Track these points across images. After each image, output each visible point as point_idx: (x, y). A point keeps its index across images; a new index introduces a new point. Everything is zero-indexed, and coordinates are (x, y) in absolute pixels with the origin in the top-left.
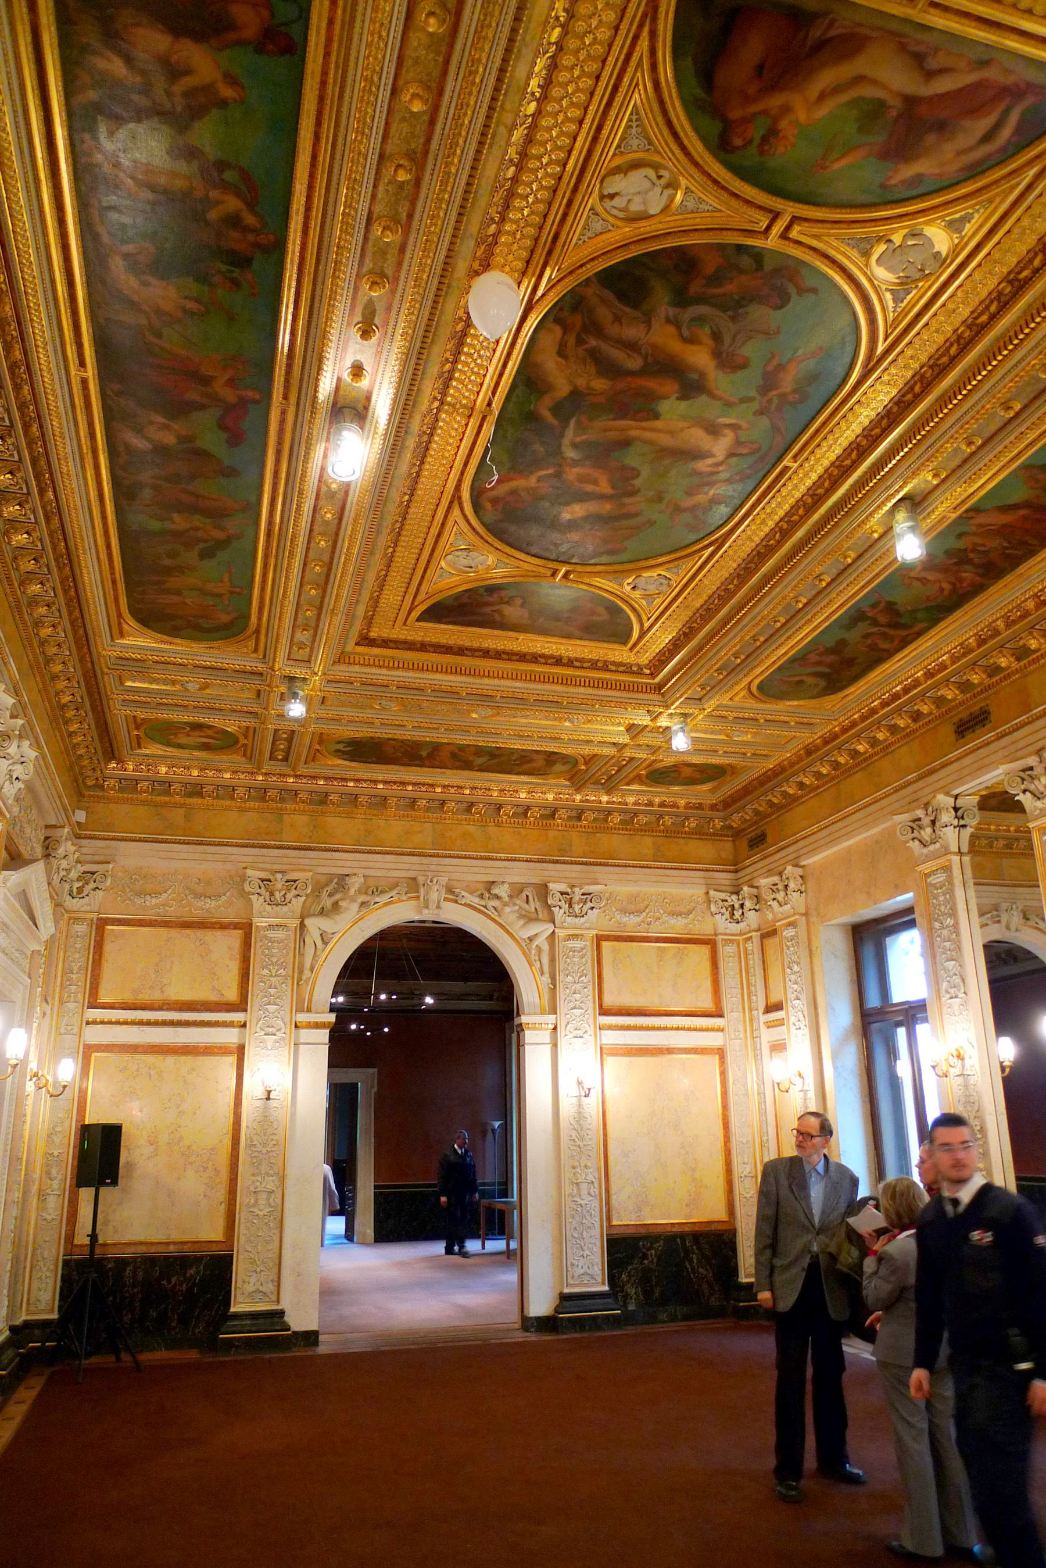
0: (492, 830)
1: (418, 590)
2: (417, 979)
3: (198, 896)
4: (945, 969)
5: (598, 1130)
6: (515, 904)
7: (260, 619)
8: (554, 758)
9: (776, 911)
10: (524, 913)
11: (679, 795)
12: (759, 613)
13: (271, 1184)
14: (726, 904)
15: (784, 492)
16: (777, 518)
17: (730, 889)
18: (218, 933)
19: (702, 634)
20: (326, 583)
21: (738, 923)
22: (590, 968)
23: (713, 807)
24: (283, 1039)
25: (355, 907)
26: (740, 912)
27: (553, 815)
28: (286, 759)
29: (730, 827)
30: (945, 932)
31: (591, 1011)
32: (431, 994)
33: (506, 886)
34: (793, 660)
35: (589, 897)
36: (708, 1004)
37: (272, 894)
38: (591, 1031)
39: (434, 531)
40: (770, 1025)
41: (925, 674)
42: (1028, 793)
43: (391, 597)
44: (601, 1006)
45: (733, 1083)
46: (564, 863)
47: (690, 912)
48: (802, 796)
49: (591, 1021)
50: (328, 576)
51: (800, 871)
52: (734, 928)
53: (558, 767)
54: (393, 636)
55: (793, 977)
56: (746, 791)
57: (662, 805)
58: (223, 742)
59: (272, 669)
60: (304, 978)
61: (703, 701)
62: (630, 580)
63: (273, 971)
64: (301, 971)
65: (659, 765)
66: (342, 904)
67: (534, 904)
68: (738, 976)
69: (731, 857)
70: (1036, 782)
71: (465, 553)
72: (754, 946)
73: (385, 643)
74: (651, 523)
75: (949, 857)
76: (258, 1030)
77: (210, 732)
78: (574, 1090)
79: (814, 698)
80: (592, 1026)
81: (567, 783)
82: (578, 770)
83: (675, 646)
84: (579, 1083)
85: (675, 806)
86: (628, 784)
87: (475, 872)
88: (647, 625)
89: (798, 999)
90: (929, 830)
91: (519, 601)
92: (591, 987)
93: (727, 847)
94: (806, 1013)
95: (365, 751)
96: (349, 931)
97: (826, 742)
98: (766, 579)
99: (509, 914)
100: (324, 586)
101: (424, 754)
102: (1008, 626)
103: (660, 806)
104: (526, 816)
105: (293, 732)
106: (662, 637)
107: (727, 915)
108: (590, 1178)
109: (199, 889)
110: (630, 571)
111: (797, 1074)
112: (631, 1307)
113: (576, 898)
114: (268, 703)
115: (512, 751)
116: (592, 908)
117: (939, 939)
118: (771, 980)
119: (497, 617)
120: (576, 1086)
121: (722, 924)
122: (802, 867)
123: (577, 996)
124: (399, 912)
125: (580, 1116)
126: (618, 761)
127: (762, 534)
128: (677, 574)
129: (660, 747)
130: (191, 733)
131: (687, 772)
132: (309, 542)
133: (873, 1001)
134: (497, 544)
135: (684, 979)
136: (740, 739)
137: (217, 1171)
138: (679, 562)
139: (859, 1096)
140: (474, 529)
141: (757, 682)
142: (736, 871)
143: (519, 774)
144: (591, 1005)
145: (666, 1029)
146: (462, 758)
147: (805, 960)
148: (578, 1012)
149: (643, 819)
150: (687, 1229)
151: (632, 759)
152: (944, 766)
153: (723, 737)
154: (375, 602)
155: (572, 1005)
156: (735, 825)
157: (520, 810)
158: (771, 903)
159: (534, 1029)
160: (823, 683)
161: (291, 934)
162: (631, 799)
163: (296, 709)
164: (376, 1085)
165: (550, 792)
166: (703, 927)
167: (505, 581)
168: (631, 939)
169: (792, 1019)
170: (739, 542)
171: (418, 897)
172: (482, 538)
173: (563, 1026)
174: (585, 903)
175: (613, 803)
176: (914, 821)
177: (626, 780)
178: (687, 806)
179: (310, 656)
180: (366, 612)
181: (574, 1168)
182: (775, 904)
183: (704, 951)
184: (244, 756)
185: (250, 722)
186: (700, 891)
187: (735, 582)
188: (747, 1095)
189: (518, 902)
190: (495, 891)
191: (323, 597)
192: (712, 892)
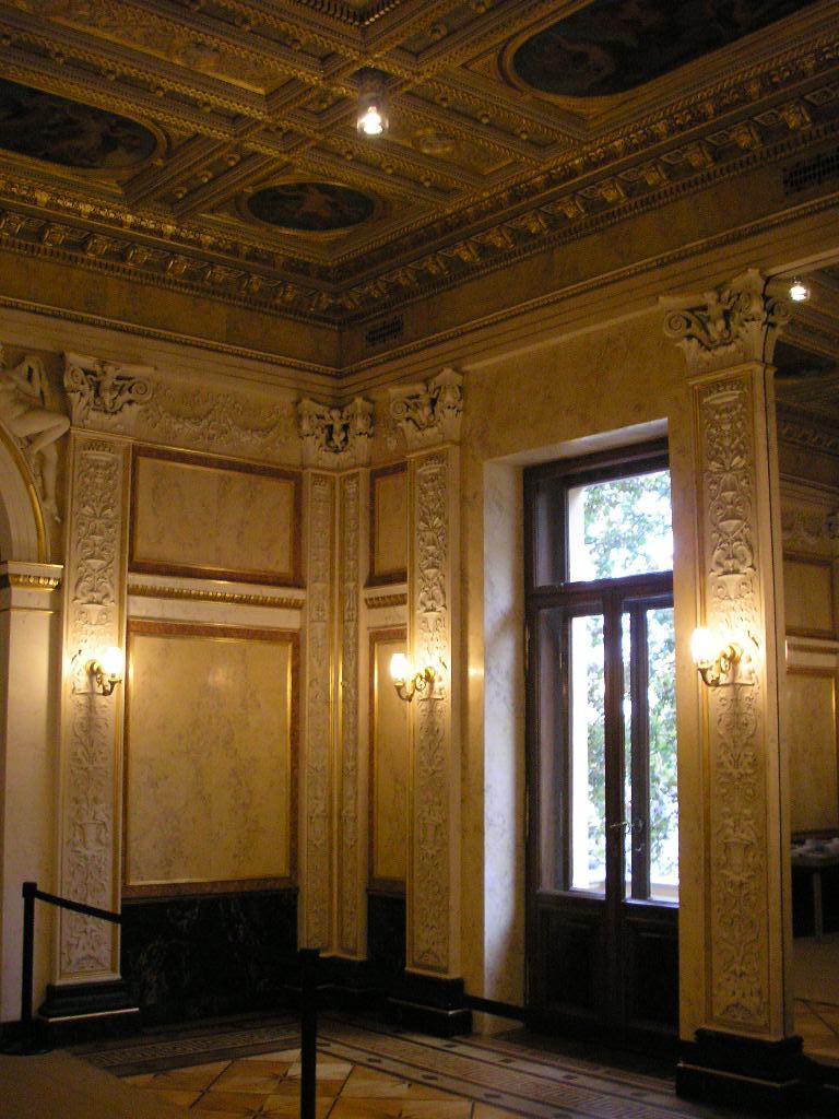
4: (721, 532)
5: (116, 745)
6: (10, 379)
10: (22, 396)
17: (330, 401)
23: (323, 274)
26: (343, 436)
27: (82, 246)
29: (343, 308)
30: (727, 477)
31: (116, 563)
35: (128, 384)
36: (282, 566)
38: (114, 596)
40: (373, 604)
41: (511, 195)
42: (411, 422)
46: (93, 324)
47: (270, 428)
49: (116, 580)
52: (329, 459)
53: (119, 157)
55: (429, 535)
61: (421, 59)
67: (40, 385)
68: (328, 531)
70: (420, 412)
72: (357, 489)
75: (747, 367)
78: (82, 682)
80: (116, 586)
81: (120, 192)
86: (212, 211)
89: (433, 566)
90: (427, 410)
92: (118, 526)
102: (718, 112)
103: (248, 257)
107: (323, 438)
108: (101, 816)
112: (150, 1001)
113: (108, 383)
116: (130, 402)
117: (713, 487)
118: (381, 542)
121: (314, 450)
123: (98, 538)
133: (543, 579)
139: (512, 709)
143: (47, 157)
144: (117, 555)
147: (453, 513)
148: (96, 563)
149: (220, 274)
150: (232, 889)
151: (255, 154)
152: (755, 232)
155: (88, 551)
156: (349, 305)
159: (28, 584)
173: (74, 581)
176: (411, 398)
183: (281, 491)
186: (287, 398)
188: (327, 702)
189: (15, 377)
192: (306, 402)
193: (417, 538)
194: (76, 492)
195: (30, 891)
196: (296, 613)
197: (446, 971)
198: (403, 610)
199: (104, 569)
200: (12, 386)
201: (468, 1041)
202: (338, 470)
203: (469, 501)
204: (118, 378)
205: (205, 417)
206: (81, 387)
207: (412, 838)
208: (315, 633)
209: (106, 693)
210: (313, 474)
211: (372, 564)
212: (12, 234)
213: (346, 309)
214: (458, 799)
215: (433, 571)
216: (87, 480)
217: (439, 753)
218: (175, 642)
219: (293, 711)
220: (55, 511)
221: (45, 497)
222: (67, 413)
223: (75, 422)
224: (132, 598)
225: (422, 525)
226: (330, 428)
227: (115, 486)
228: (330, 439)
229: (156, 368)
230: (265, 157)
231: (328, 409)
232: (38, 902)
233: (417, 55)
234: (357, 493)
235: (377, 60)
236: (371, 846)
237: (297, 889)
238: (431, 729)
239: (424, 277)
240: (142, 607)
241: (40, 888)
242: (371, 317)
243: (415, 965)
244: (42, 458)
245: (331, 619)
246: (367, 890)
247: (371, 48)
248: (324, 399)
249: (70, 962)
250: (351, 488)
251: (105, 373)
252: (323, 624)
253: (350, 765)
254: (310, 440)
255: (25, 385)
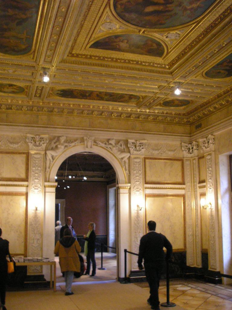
0: (109, 121)
1: (91, 37)
2: (81, 171)
3: (11, 143)
5: (144, 221)
6: (117, 146)
7: (35, 47)
8: (132, 97)
9: (205, 150)
11: (173, 110)
12: (210, 48)
13: (38, 236)
14: (187, 147)
15: (224, 4)
16: (220, 14)
17: (189, 142)
18: (18, 156)
19: (189, 54)
20: (60, 34)
21: (191, 154)
22: (142, 167)
23: (184, 115)
24: (40, 191)
25: (63, 147)
26: (192, 150)
27: (130, 117)
28: (40, 96)
29: (189, 122)
31: (142, 183)
32: (86, 176)
33: (114, 140)
34: (218, 65)
35: (142, 145)
37: (35, 143)
38: (142, 189)
39: (99, 15)
40: (200, 187)
43: (81, 39)
44: (145, 181)
45: (188, 206)
46: (134, 133)
47: (175, 150)
48: (215, 112)
49: (142, 186)
50: (61, 32)
51: (213, 137)
52: (189, 155)
53: (133, 100)
54: (81, 53)
55: (209, 172)
56: (196, 109)
57: (167, 113)
58: (21, 90)
59: (38, 65)
60: (47, 170)
62: (166, 34)
63: (37, 168)
64: (46, 169)
65: (168, 100)
66: (59, 146)
67: (123, 147)
69: (189, 132)
71: (109, 23)
72: (196, 162)
73: (77, 56)
74: (176, 14)
76: (32, 188)
77: (15, 87)
78: (136, 208)
79: (223, 78)
81: (135, 105)
82: (139, 100)
83: (178, 58)
84: (138, 206)
85: (171, 114)
86: (156, 106)
87: (104, 135)
88: (169, 50)
89: (210, 179)
90: (207, 144)
91: (126, 41)
92: (142, 175)
93: (188, 128)
94: (213, 184)
95: (67, 94)
96: (61, 155)
97: (225, 93)
98: (214, 35)
99: (115, 150)
100: (60, 34)
101: (87, 95)
104: (112, 116)
105: (43, 87)
106: (173, 56)
107: (187, 151)
109: (12, 141)
110: (166, 31)
111: (209, 203)
113: (138, 145)
114: (36, 77)
115: (118, 94)
116: (143, 148)
118: (201, 173)
119: (118, 47)
120: (137, 207)
121: (186, 154)
122: (214, 135)
123: (138, 178)
124: (77, 149)
125: (138, 216)
126: (154, 98)
127: (214, 19)
128: (183, 33)
129: (169, 94)
130: (9, 88)
131: (176, 102)
132: (55, 19)
134: (121, 20)
135: (172, 172)
136: (196, 91)
137: (21, 233)
138: (184, 28)
140: (113, 15)
141: (205, 72)
142: (191, 136)
143: (119, 102)
144: (142, 181)
145: (166, 188)
146: (100, 96)
147: (214, 166)
149: (160, 118)
151: (158, 97)
153: (191, 91)
154: (75, 40)
155: (136, 180)
156: (191, 121)
157: (100, 113)
158: (203, 147)
159: (123, 188)
160: (227, 73)
161: (42, 156)
162: (156, 111)
163: (46, 79)
164: (65, 205)
165: (130, 108)
166: (179, 155)
167: (122, 33)
168: (155, 159)
169: (208, 185)
170: (206, 22)
171: (84, 144)
172: (116, 18)
173: (133, 187)
174: (140, 146)
175: (150, 112)
177: (156, 105)
178: (175, 114)
179: (52, 60)
180: (72, 44)
181: (135, 232)
182: (204, 148)
183: (179, 164)
184: (26, 95)
185: (28, 84)
186: (178, 143)
187: (202, 36)
190: (110, 142)
191: (58, 39)
192: (183, 144)
193: (207, 172)
194: (132, 168)
195: (126, 251)
196: (184, 190)
197: (216, 269)
198: (205, 188)
199: (139, 184)
200: (117, 148)
201: (220, 285)
202: (192, 157)
203: (217, 164)
204: (140, 143)
205: (160, 149)
206: (132, 146)
207: (209, 239)
208: (188, 195)
209: (140, 210)
210: (186, 159)
211: (200, 179)
212: (115, 116)
213: (190, 121)
214: (217, 231)
215: (211, 180)
216: (135, 165)
217: (213, 221)
218: (156, 198)
219: (184, 212)
220: (128, 172)
221: (126, 170)
222: (129, 152)
223: (131, 153)
224: (146, 189)
225: (208, 170)
226: (189, 149)
227: (141, 166)
228: (189, 151)
229: (148, 140)
230: (161, 97)
231: (188, 144)
232: (127, 254)
233: (185, 77)
234: (196, 162)
235: (177, 80)
236: (202, 242)
237: (186, 251)
238: (212, 216)
239: (204, 114)
240: (148, 191)
241: (128, 250)
242: (196, 123)
243: (211, 268)
244: (125, 162)
245: (192, 191)
246: (201, 252)
247: (174, 78)
248: (187, 142)
249: (135, 266)
250: (194, 161)
251: (137, 143)
252: (190, 193)
253: (197, 223)
254: (184, 152)
255: (120, 147)
